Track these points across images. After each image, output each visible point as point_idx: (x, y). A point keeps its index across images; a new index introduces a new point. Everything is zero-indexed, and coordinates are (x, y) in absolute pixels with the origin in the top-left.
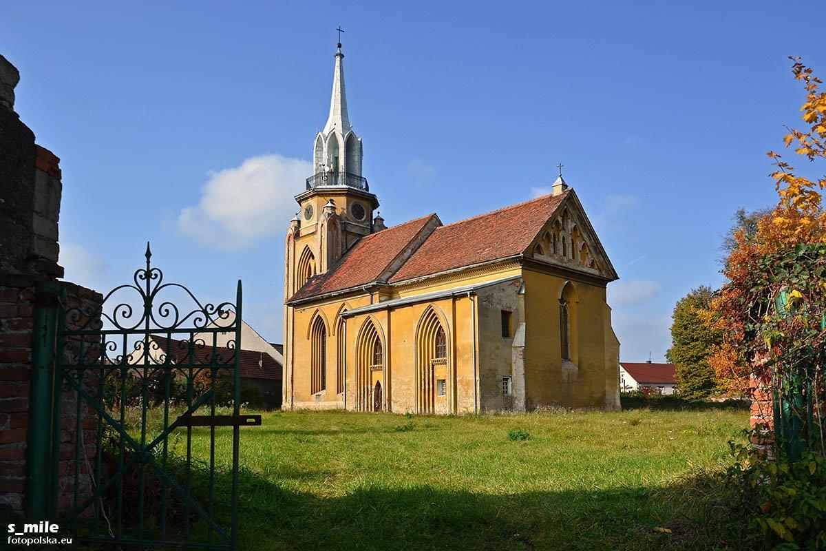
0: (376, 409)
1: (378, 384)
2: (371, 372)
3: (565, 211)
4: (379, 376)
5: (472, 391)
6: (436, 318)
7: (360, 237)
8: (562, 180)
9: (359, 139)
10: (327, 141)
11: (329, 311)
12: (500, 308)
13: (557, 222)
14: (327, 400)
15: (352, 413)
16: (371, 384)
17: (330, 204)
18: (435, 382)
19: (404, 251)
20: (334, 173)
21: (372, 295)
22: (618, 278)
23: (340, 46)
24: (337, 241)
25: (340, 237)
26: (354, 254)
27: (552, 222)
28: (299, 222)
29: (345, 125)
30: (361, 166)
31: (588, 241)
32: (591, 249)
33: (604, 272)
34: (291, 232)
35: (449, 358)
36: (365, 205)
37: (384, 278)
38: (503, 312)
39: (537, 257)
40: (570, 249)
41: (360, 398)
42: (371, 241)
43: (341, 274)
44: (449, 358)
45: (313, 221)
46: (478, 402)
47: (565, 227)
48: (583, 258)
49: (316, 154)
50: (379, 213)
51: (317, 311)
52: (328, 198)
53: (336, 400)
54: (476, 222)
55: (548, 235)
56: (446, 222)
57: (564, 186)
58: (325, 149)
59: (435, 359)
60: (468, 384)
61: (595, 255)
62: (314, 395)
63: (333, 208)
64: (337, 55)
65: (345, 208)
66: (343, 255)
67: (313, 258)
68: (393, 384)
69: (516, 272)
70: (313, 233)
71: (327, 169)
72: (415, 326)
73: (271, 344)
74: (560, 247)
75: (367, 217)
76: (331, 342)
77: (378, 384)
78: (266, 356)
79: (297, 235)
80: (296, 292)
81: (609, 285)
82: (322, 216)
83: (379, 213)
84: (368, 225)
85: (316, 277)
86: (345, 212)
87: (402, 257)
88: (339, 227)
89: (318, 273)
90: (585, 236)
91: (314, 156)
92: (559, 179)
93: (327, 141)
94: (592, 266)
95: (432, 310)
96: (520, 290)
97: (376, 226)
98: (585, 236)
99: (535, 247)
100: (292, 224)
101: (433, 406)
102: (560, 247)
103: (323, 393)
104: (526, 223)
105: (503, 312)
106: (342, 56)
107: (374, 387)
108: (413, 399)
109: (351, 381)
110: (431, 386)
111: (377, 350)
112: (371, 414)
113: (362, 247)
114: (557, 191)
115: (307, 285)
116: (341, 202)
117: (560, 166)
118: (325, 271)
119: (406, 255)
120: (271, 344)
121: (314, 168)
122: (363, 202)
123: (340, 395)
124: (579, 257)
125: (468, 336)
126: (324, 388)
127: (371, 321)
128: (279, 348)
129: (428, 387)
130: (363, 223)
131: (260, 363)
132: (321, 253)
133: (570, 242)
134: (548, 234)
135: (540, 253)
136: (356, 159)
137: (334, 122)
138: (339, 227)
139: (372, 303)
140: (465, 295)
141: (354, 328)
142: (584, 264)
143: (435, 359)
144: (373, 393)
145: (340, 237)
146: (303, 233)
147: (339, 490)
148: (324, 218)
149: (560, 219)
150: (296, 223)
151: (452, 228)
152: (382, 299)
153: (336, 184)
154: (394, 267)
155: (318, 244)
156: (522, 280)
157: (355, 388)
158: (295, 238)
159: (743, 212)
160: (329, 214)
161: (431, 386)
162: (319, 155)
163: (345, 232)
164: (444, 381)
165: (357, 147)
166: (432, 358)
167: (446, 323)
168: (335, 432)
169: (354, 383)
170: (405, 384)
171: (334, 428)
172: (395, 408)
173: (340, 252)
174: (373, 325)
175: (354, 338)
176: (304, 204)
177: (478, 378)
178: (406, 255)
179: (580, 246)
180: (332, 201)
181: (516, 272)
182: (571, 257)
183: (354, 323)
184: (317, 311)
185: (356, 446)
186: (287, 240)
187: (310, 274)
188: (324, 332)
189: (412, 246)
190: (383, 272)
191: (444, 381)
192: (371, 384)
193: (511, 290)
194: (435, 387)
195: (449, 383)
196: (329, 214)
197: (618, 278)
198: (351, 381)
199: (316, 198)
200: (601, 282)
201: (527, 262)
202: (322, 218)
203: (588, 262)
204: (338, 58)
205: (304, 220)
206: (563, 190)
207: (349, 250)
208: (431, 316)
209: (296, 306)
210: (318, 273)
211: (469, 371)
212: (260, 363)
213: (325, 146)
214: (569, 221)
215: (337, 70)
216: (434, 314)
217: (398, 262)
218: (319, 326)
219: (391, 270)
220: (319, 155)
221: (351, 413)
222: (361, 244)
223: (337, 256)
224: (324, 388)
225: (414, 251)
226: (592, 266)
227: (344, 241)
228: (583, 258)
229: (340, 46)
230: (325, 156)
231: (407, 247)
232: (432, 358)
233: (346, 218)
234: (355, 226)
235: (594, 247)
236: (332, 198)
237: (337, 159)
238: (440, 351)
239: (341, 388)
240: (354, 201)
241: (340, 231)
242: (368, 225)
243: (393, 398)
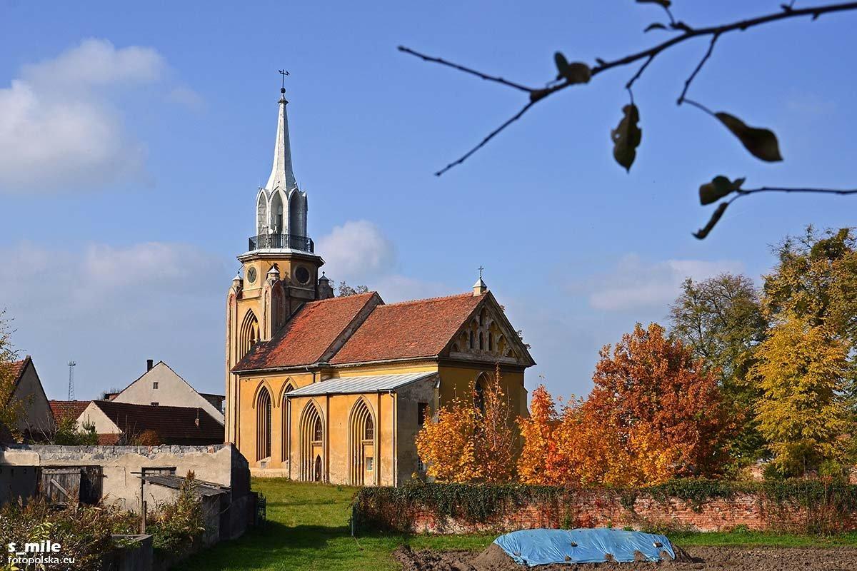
0: (317, 479)
1: (319, 458)
2: (313, 447)
3: (484, 309)
4: (319, 451)
5: (391, 469)
6: (366, 407)
7: (304, 302)
8: (482, 281)
9: (304, 195)
10: (271, 200)
11: (275, 384)
12: (417, 401)
13: (475, 321)
14: (272, 467)
15: (296, 483)
16: (313, 458)
17: (273, 270)
18: (365, 459)
19: (345, 331)
20: (276, 239)
21: (315, 374)
22: (535, 364)
23: (283, 91)
24: (281, 308)
25: (284, 303)
26: (299, 323)
27: (471, 320)
28: (242, 281)
29: (290, 180)
30: (306, 213)
31: (505, 333)
32: (509, 340)
33: (522, 359)
34: (232, 292)
35: (375, 440)
36: (308, 266)
37: (325, 358)
38: (419, 404)
39: (454, 355)
40: (487, 343)
41: (303, 469)
42: (316, 310)
43: (284, 346)
44: (375, 440)
45: (257, 285)
46: (396, 477)
47: (483, 323)
48: (501, 348)
49: (259, 211)
50: (324, 273)
51: (262, 382)
52: (272, 263)
53: (280, 468)
54: (410, 308)
55: (465, 334)
56: (388, 301)
57: (483, 287)
58: (269, 209)
59: (365, 440)
60: (389, 463)
61: (513, 345)
62: (259, 462)
63: (277, 274)
64: (281, 102)
65: (289, 272)
66: (288, 321)
67: (256, 321)
68: (331, 459)
69: (433, 369)
70: (256, 298)
71: (271, 232)
72: (349, 412)
73: (201, 394)
74: (477, 343)
75: (312, 280)
76: (276, 413)
77: (319, 458)
78: (201, 413)
79: (240, 296)
80: (238, 361)
81: (527, 369)
82: (266, 282)
83: (324, 273)
84: (312, 288)
85: (260, 343)
86: (289, 276)
87: (343, 337)
88: (283, 293)
89: (262, 339)
90: (503, 330)
91: (257, 214)
92: (479, 281)
93: (271, 200)
94: (510, 355)
95: (362, 401)
96: (436, 384)
97: (322, 290)
98: (503, 330)
99: (452, 346)
100: (234, 283)
101: (363, 479)
102: (477, 343)
103: (268, 460)
104: (448, 322)
105: (419, 404)
106: (285, 102)
107: (315, 460)
108: (346, 473)
109: (295, 453)
110: (361, 462)
111: (317, 428)
112: (311, 483)
113: (307, 316)
114: (477, 292)
115: (252, 352)
116: (285, 266)
117: (481, 269)
118: (269, 339)
119: (347, 334)
120: (201, 394)
121: (257, 226)
122: (307, 265)
123: (284, 463)
124: (497, 348)
125: (389, 425)
126: (269, 455)
127: (312, 404)
128: (217, 401)
129: (359, 463)
130: (307, 287)
131: (197, 422)
132: (265, 319)
133: (487, 336)
134: (465, 334)
135: (456, 351)
136: (301, 217)
137: (276, 180)
138: (283, 293)
139: (314, 382)
140: (388, 392)
141: (298, 408)
142: (501, 354)
143: (365, 440)
144: (314, 465)
145: (284, 303)
146: (246, 295)
147: (294, 525)
148: (268, 285)
149: (477, 319)
150: (239, 282)
151: (392, 309)
152: (323, 378)
153: (279, 247)
154: (335, 347)
155: (262, 309)
156: (438, 376)
157: (299, 461)
158: (237, 299)
159: (690, 282)
160: (273, 281)
161: (361, 462)
162: (262, 212)
163: (289, 298)
164: (372, 458)
165: (302, 204)
166: (363, 439)
167: (373, 411)
168: (286, 505)
169: (298, 456)
170: (341, 459)
171: (285, 501)
172: (333, 480)
173: (284, 320)
174: (314, 407)
175: (298, 417)
176: (247, 265)
177: (396, 459)
178: (347, 334)
179: (497, 338)
180: (275, 266)
181: (433, 369)
182: (487, 350)
183: (298, 403)
184: (262, 382)
185: (299, 513)
186: (229, 300)
187: (253, 337)
188: (269, 401)
189: (352, 326)
190: (325, 354)
191: (372, 458)
192: (313, 458)
193: (427, 386)
194: (365, 463)
195: (375, 462)
196: (273, 281)
197: (535, 364)
198: (295, 453)
199: (260, 262)
200: (520, 370)
201: (443, 360)
202: (266, 284)
203: (505, 352)
204: (282, 105)
205: (246, 282)
206: (481, 291)
207: (293, 316)
208: (361, 406)
209: (242, 375)
210: (262, 339)
211: (389, 453)
212: (197, 422)
213: (269, 205)
214: (487, 318)
215: (281, 118)
216: (364, 404)
217: (339, 342)
218: (264, 397)
219: (333, 351)
220: (262, 212)
221: (295, 484)
222: (305, 312)
223: (282, 322)
224: (269, 455)
225: (355, 330)
226: (510, 355)
227: (289, 307)
228: (501, 348)
229: (283, 91)
230: (269, 216)
231: (348, 327)
232: (363, 439)
233: (290, 282)
234: (300, 290)
235: (511, 338)
236: (276, 262)
237: (280, 217)
238: (369, 434)
239: (285, 456)
240: (299, 264)
241: (284, 298)
242: (312, 288)
243: (330, 470)
